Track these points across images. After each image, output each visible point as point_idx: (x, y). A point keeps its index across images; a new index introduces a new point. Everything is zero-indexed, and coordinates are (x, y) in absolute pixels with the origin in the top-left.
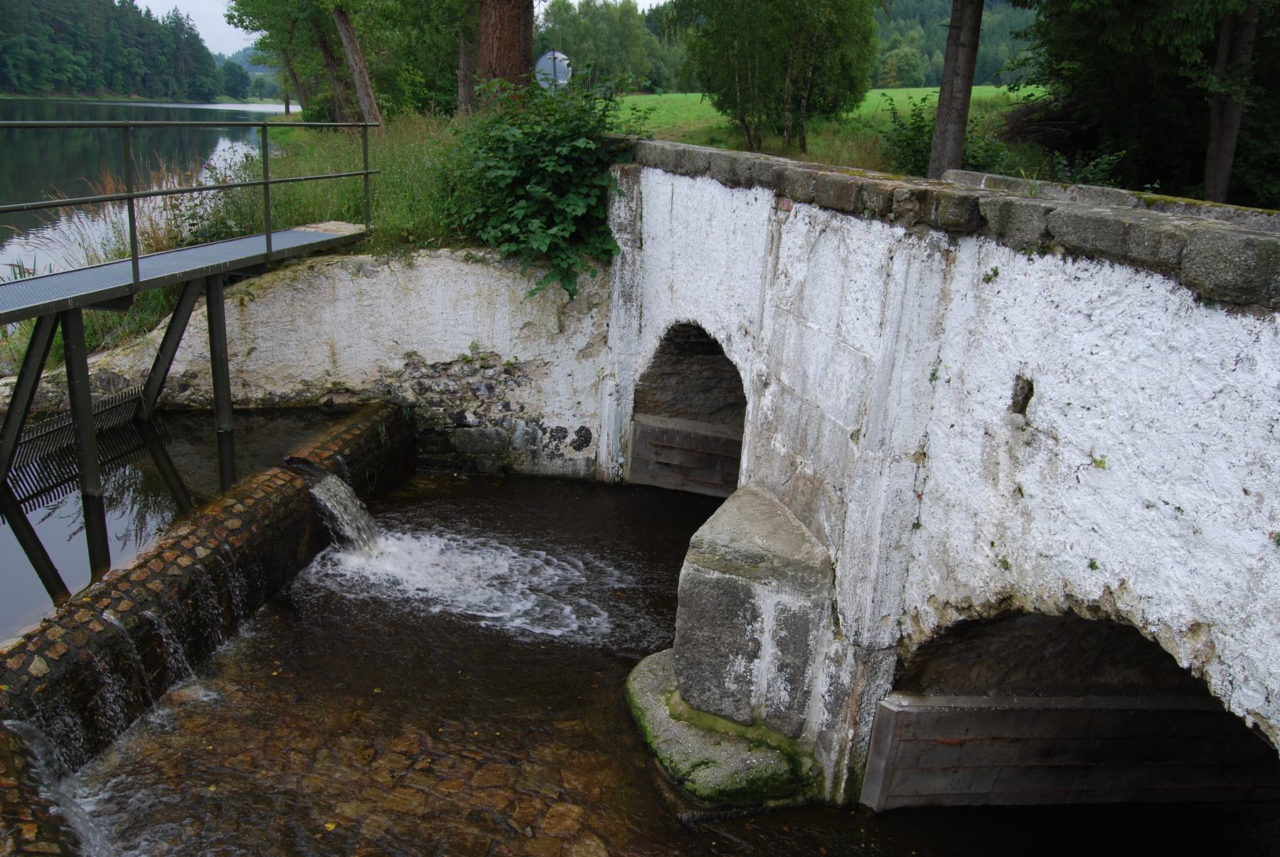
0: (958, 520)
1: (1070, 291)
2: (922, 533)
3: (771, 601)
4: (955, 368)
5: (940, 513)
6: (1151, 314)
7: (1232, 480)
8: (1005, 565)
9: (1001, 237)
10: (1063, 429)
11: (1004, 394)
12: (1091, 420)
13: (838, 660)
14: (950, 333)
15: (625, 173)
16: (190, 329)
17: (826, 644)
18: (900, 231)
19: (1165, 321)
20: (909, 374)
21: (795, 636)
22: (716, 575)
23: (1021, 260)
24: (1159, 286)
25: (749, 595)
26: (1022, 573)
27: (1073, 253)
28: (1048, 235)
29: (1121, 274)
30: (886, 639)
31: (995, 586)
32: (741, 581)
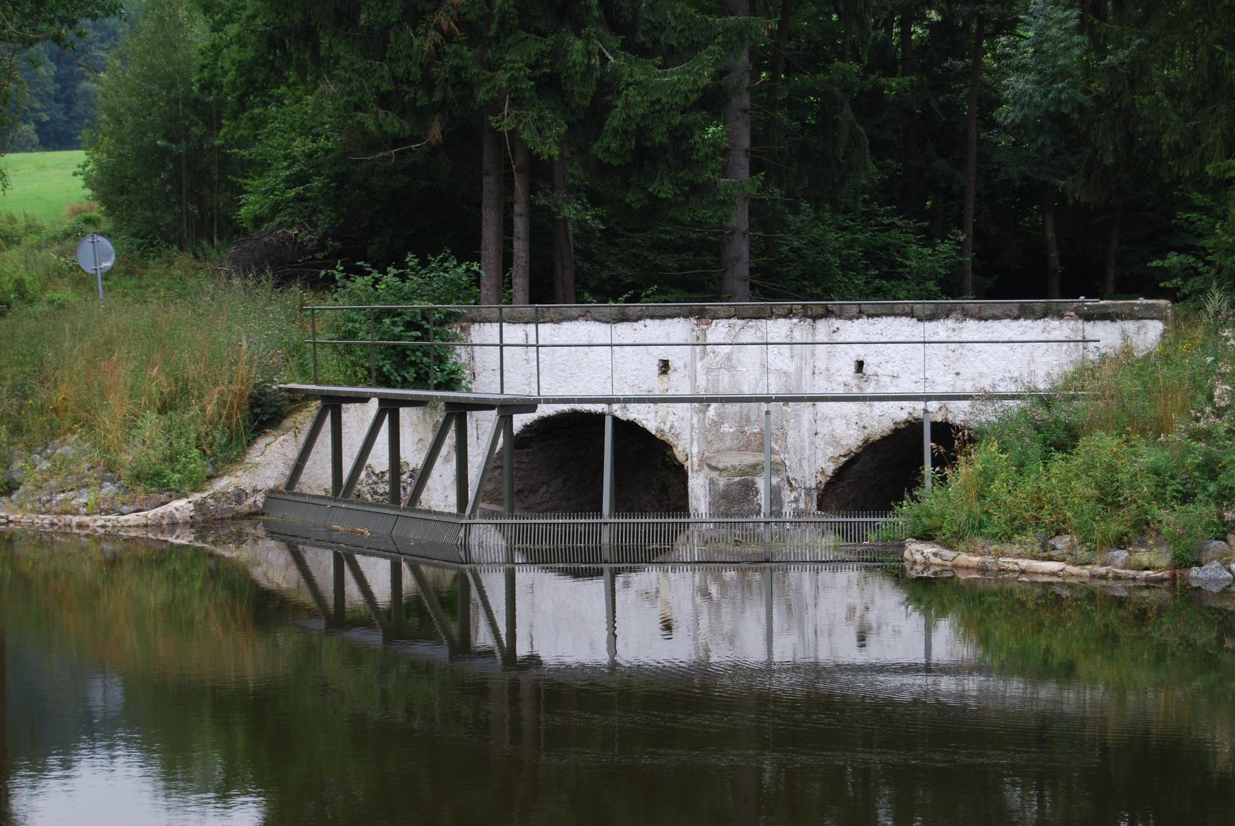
0: (837, 422)
1: (872, 328)
2: (820, 435)
4: (824, 367)
5: (827, 424)
6: (903, 329)
7: (940, 364)
8: (865, 428)
9: (839, 317)
10: (880, 371)
11: (853, 368)
12: (889, 365)
13: (796, 500)
14: (818, 356)
15: (463, 329)
16: (323, 430)
17: (788, 496)
18: (795, 321)
20: (807, 372)
21: (775, 496)
22: (738, 479)
23: (849, 323)
25: (754, 483)
26: (872, 426)
30: (814, 486)
31: (861, 438)
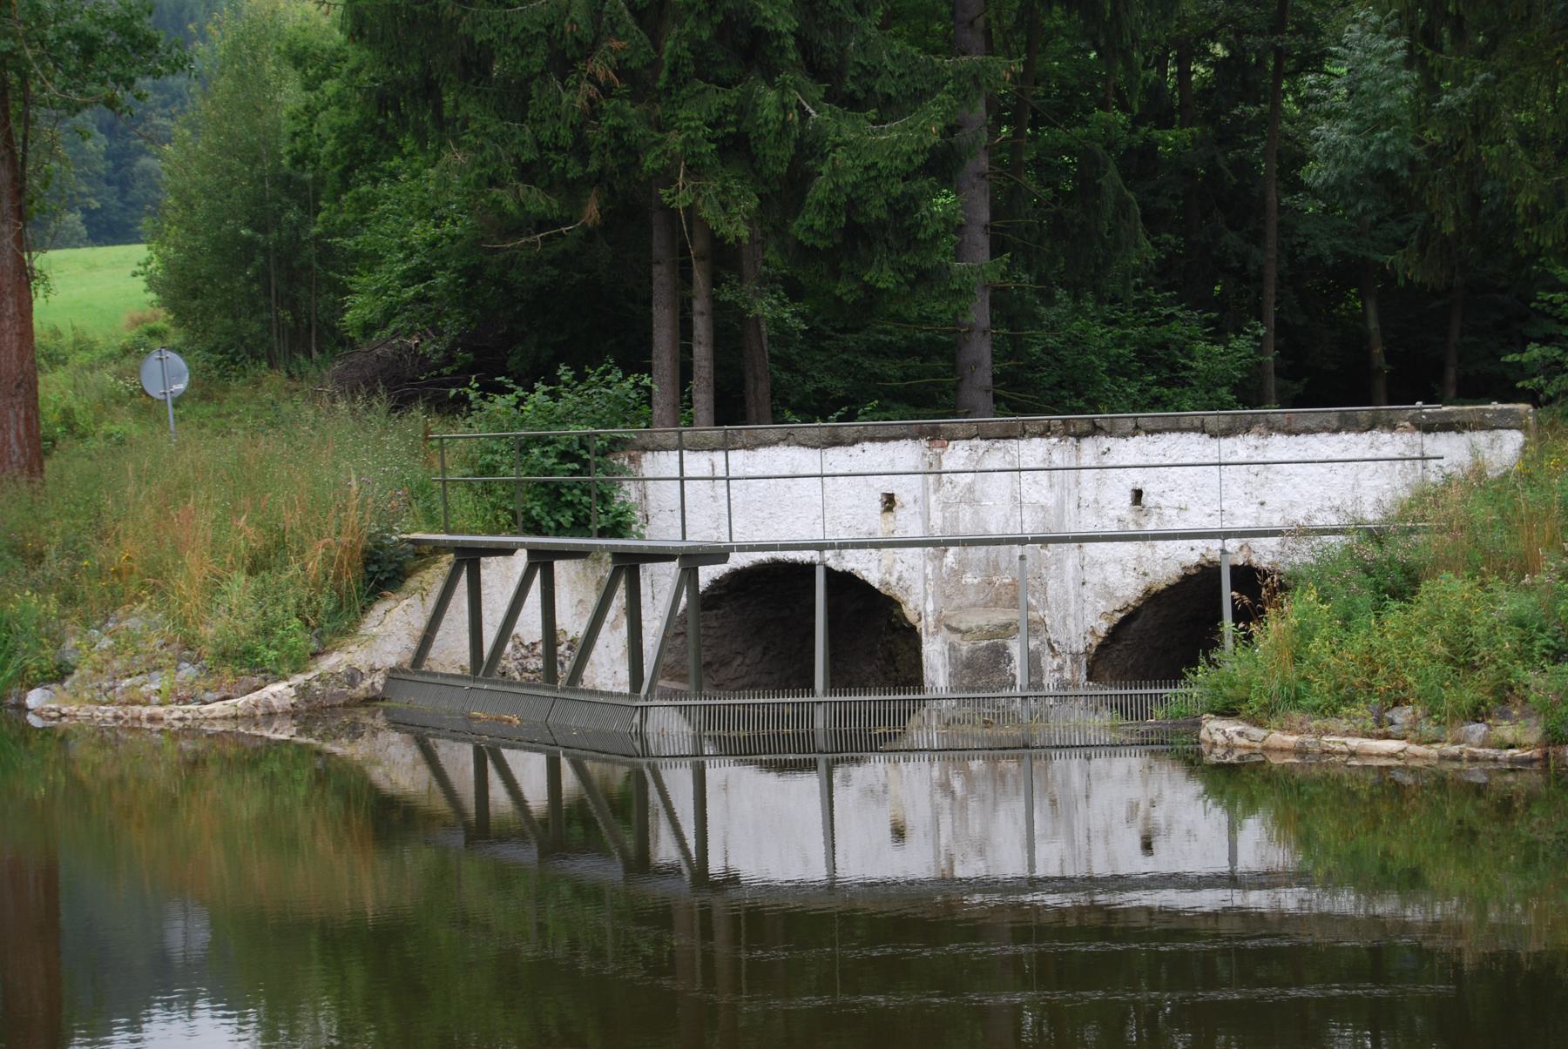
0: (1110, 568)
1: (1152, 447)
2: (1089, 586)
3: (1015, 648)
7: (1240, 492)
8: (1145, 574)
9: (1110, 434)
10: (1163, 502)
12: (1175, 495)
13: (1060, 669)
14: (1084, 484)
16: (457, 591)
17: (1049, 663)
18: (1054, 440)
19: (1200, 448)
23: (1123, 441)
24: (1193, 436)
25: (1005, 648)
26: (1155, 573)
27: (1149, 432)
28: (1137, 427)
29: (1175, 436)
30: (1082, 649)
31: (1142, 587)
32: (1000, 641)
